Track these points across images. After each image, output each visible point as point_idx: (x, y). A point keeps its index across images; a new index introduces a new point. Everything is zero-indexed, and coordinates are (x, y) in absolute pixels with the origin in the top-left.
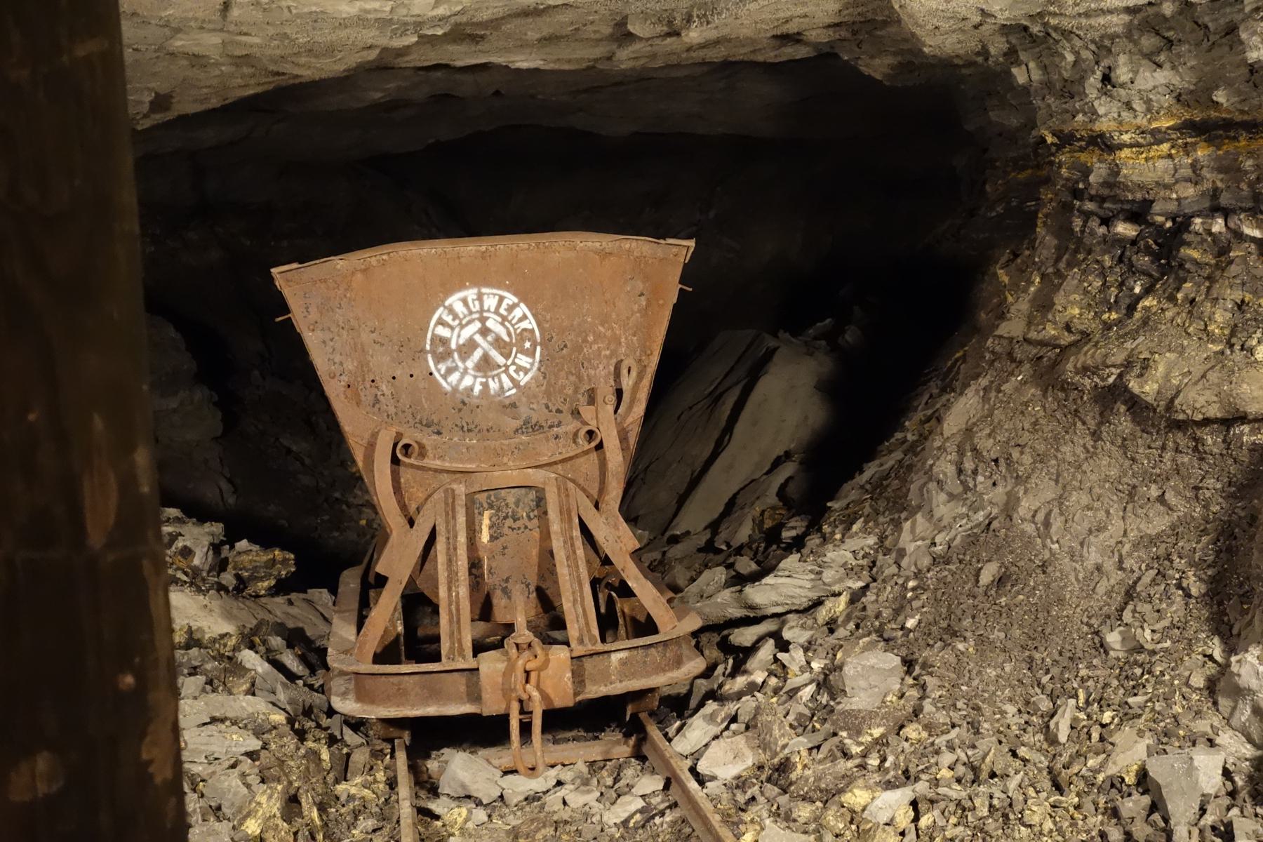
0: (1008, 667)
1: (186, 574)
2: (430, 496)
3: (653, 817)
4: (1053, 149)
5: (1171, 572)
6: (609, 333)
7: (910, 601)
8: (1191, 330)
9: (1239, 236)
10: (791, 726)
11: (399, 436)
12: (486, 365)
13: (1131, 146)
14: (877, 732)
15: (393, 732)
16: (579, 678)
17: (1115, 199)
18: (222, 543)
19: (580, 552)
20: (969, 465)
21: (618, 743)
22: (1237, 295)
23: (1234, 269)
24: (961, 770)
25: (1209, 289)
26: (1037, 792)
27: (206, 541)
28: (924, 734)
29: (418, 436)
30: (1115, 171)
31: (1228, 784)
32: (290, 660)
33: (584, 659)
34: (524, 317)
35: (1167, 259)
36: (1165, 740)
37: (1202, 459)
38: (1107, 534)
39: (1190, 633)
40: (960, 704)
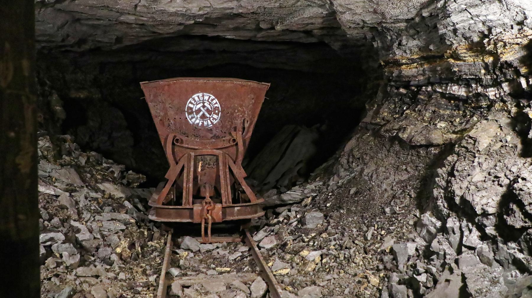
0: (355, 218)
1: (112, 178)
2: (183, 156)
3: (244, 258)
4: (383, 67)
5: (406, 190)
6: (242, 110)
7: (329, 198)
8: (419, 119)
9: (435, 91)
10: (288, 233)
11: (175, 136)
12: (203, 117)
13: (405, 64)
14: (313, 235)
15: (168, 229)
16: (224, 214)
17: (400, 81)
18: (125, 171)
19: (228, 176)
20: (351, 160)
21: (237, 238)
22: (433, 109)
23: (433, 101)
24: (337, 246)
25: (425, 107)
26: (359, 254)
27: (119, 170)
28: (327, 236)
29: (181, 137)
30: (400, 72)
31: (417, 253)
32: (140, 206)
33: (226, 209)
34: (216, 103)
35: (414, 100)
36: (399, 239)
37: (419, 158)
38: (389, 180)
39: (410, 208)
40: (339, 228)
